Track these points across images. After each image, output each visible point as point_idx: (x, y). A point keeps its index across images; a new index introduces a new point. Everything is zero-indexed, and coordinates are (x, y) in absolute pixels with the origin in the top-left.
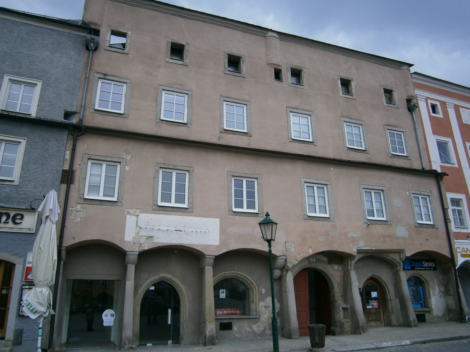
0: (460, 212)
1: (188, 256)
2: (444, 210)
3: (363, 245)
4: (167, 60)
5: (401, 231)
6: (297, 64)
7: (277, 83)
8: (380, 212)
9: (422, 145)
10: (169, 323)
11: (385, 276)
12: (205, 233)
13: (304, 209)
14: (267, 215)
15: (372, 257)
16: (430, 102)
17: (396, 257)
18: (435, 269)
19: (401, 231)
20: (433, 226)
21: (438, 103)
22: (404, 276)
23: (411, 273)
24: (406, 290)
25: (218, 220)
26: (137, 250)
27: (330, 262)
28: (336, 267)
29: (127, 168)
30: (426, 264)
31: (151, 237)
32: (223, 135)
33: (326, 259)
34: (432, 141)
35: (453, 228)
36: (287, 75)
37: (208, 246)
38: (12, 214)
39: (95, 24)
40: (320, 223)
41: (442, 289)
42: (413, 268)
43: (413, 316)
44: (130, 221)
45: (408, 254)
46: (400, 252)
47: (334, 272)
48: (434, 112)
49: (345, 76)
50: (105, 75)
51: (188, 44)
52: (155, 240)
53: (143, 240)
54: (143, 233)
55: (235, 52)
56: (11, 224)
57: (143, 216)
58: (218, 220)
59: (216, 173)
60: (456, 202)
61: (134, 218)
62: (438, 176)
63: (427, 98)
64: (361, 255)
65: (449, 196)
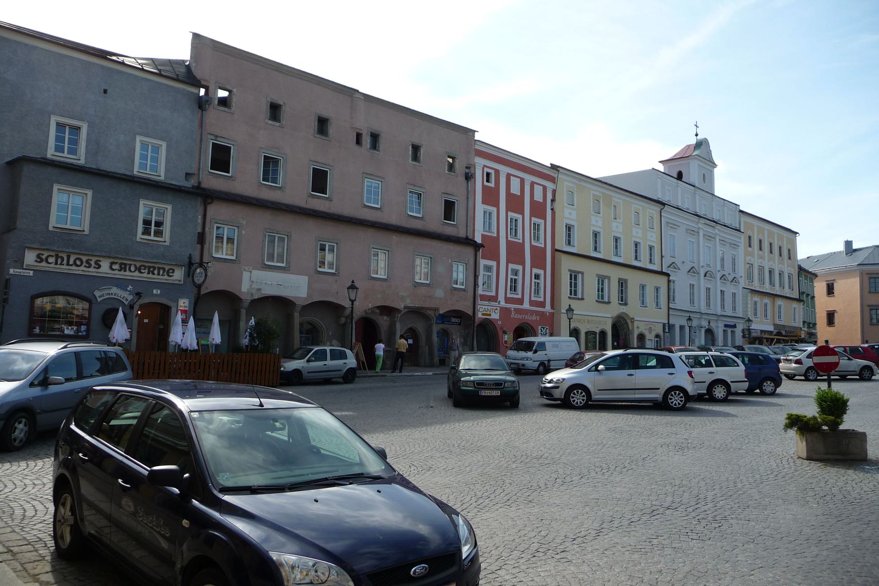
0: (489, 277)
1: (282, 303)
2: (476, 277)
3: (409, 303)
4: (267, 121)
5: (439, 293)
6: (376, 128)
7: (356, 147)
8: (331, 265)
9: (470, 214)
10: (195, 502)
11: (420, 327)
12: (296, 287)
13: (369, 271)
14: (353, 282)
15: (417, 312)
16: (486, 170)
17: (431, 313)
18: (460, 324)
19: (439, 293)
20: (464, 290)
21: (492, 172)
22: (435, 329)
23: (441, 326)
24: (435, 338)
25: (306, 278)
26: (249, 298)
27: (382, 314)
28: (385, 318)
29: (243, 232)
30: (453, 320)
31: (260, 289)
32: (310, 200)
33: (378, 311)
34: (480, 208)
35: (480, 291)
36: (367, 140)
37: (298, 298)
38: (167, 268)
39: (205, 80)
40: (379, 283)
41: (462, 340)
42: (443, 323)
43: (436, 360)
44: (246, 275)
45: (441, 312)
46: (436, 310)
47: (383, 321)
48: (488, 181)
49: (417, 142)
50: (217, 136)
51: (284, 103)
52: (263, 292)
53: (254, 292)
54: (255, 286)
55: (325, 114)
56: (166, 277)
57: (255, 272)
58: (306, 278)
59: (305, 236)
60: (488, 269)
61: (249, 273)
62: (476, 246)
63: (485, 166)
64: (406, 310)
65: (483, 262)
